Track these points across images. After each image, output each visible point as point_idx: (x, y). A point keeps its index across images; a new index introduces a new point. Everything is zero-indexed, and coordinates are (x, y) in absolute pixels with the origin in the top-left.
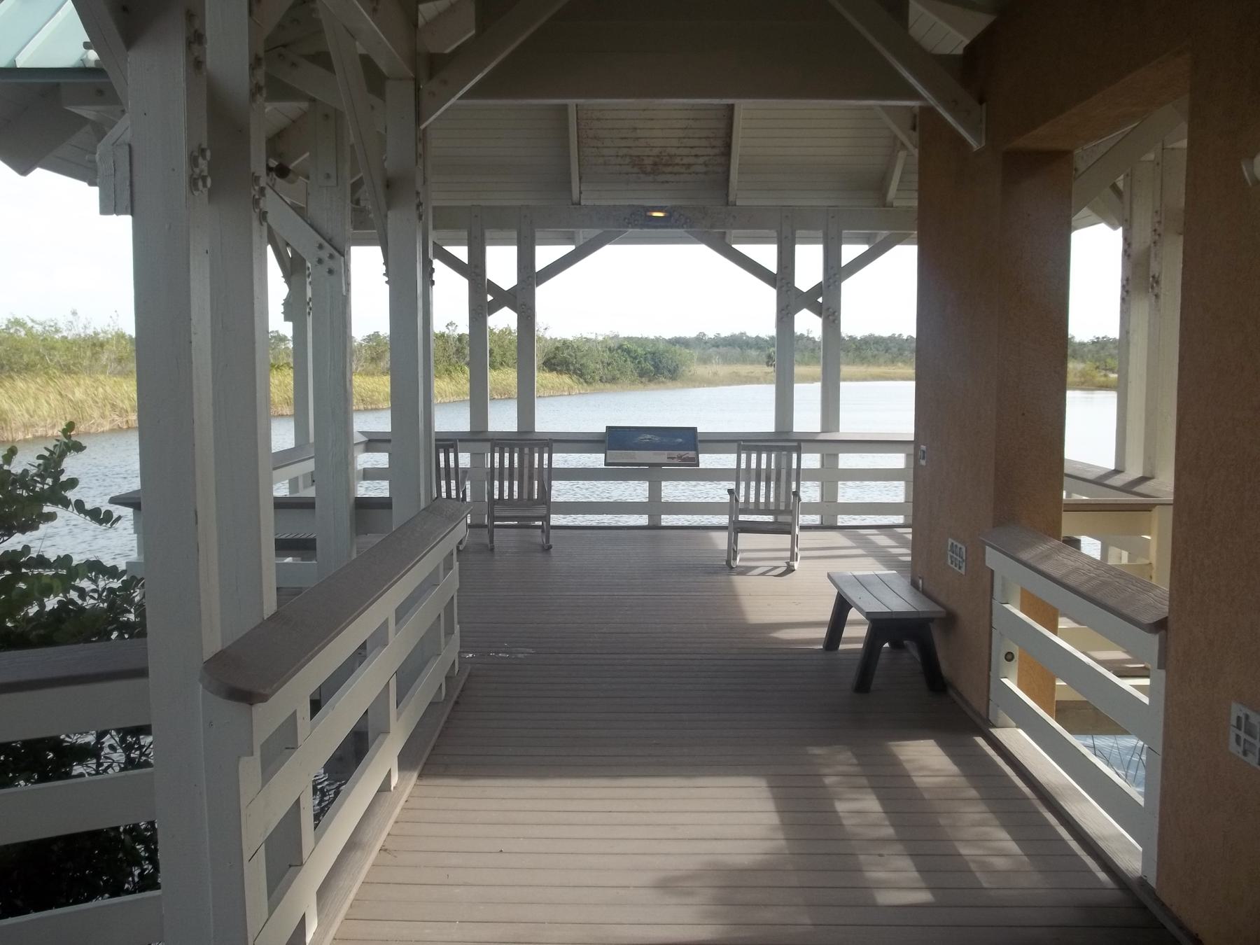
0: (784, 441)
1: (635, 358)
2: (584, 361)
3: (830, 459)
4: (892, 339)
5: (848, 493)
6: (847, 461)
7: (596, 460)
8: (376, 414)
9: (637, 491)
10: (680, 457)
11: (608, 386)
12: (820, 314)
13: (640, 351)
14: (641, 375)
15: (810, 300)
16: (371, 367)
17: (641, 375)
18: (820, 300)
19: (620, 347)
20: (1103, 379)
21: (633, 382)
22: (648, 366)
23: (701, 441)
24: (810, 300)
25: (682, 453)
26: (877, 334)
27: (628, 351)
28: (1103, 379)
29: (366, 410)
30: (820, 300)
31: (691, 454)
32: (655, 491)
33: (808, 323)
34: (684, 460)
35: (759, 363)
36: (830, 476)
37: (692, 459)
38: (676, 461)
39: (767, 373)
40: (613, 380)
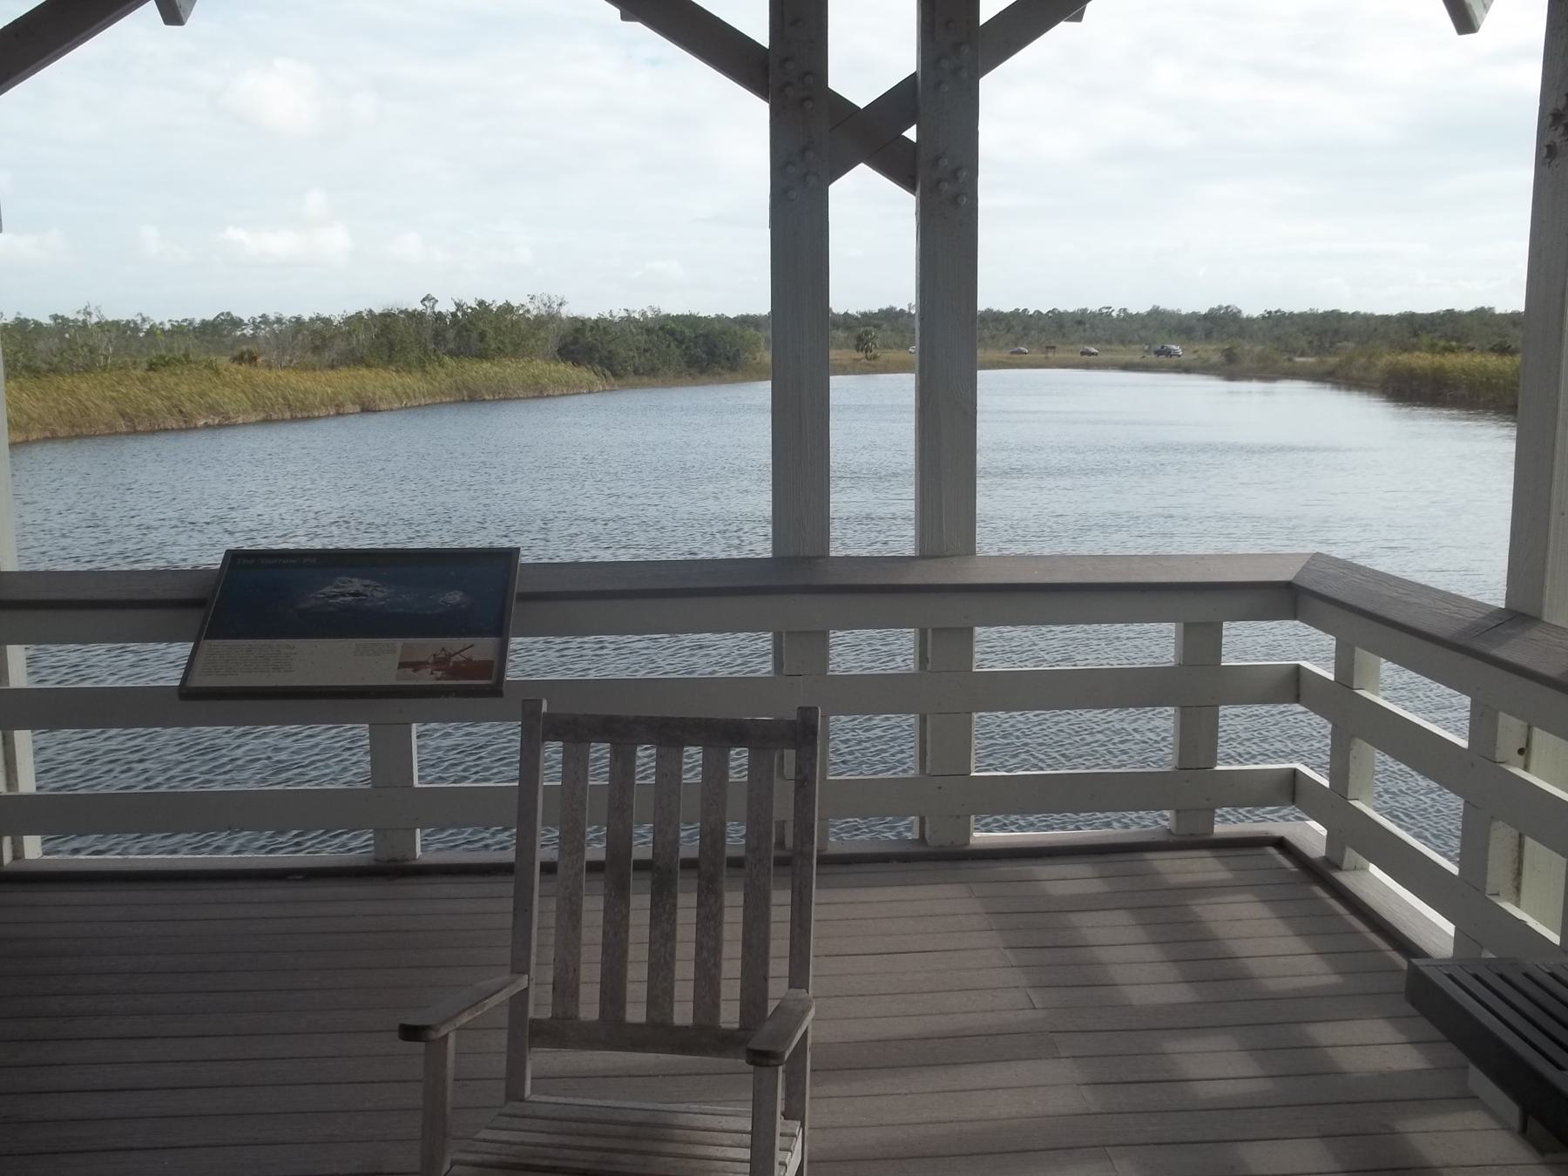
0: (796, 579)
1: (681, 342)
2: (612, 347)
3: (946, 646)
4: (1015, 314)
5: (1005, 744)
6: (1000, 648)
7: (162, 663)
8: (308, 426)
9: (332, 754)
10: (441, 663)
11: (645, 379)
12: (907, 182)
13: (687, 332)
14: (689, 365)
15: (873, 135)
16: (310, 358)
17: (689, 365)
18: (911, 134)
19: (662, 328)
20: (1287, 364)
21: (678, 375)
22: (699, 352)
23: (525, 597)
24: (873, 135)
25: (453, 644)
26: (995, 309)
27: (672, 333)
28: (1287, 364)
29: (294, 419)
30: (911, 134)
31: (481, 648)
32: (390, 757)
33: (872, 235)
34: (457, 671)
35: (848, 347)
36: (946, 694)
37: (483, 669)
38: (426, 678)
39: (856, 360)
40: (652, 372)
